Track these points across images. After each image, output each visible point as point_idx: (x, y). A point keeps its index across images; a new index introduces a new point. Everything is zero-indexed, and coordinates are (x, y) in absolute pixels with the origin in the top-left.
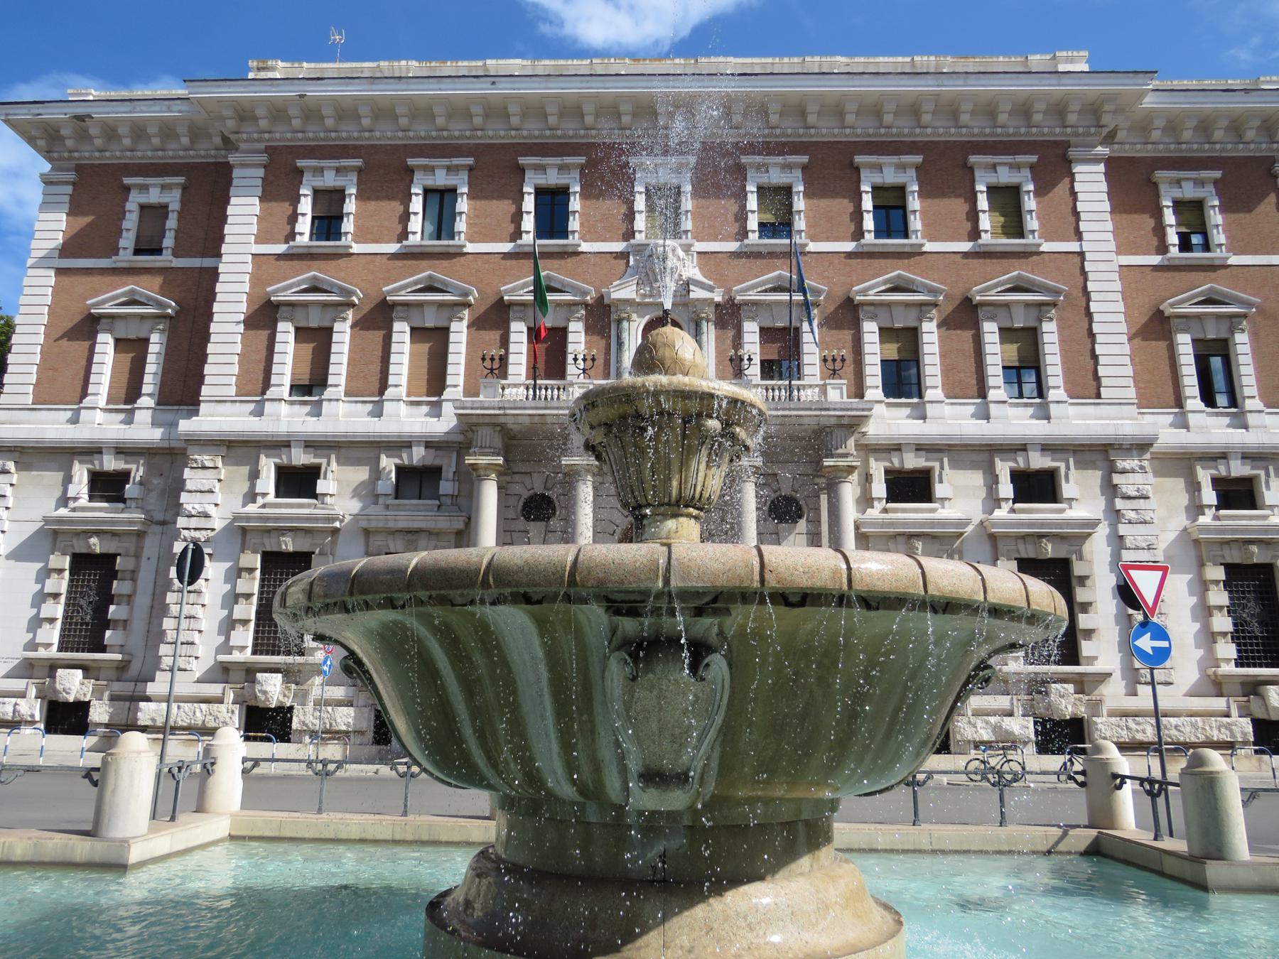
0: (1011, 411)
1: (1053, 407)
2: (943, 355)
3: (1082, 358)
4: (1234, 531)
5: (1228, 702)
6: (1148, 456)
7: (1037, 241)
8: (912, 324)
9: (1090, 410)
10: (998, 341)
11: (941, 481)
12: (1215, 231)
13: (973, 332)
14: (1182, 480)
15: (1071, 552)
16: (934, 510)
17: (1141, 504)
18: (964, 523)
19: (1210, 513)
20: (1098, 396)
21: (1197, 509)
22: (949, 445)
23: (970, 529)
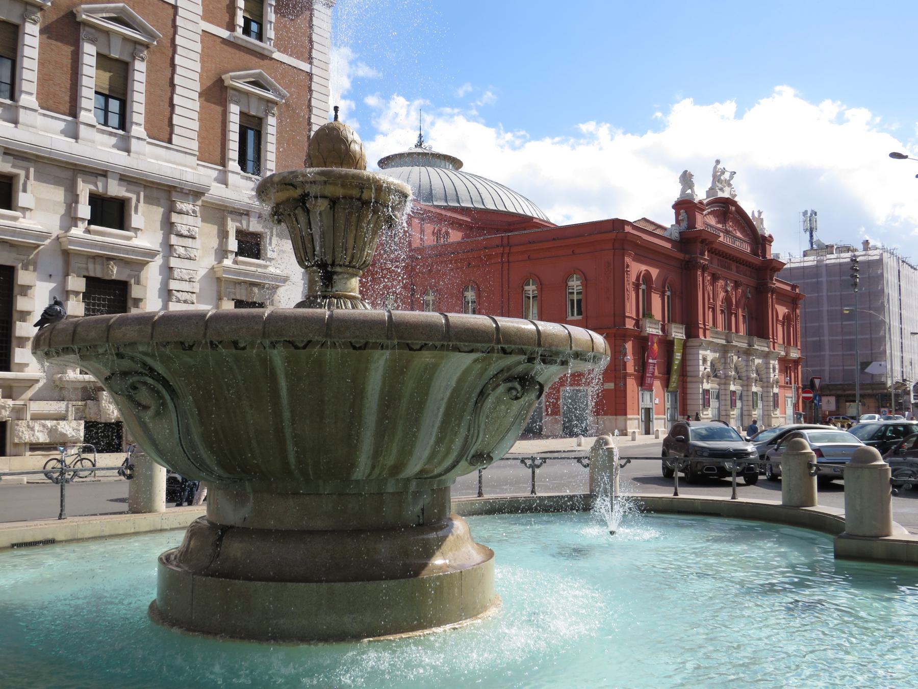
0: (100, 137)
1: (134, 142)
2: (41, 63)
3: (162, 103)
4: (246, 275)
5: (67, 407)
6: (199, 203)
7: (272, 48)
8: (15, 20)
9: (162, 152)
10: (94, 65)
11: (25, 191)
12: (269, 26)
13: (72, 48)
14: (216, 227)
15: (130, 276)
16: (15, 219)
17: (189, 242)
18: (43, 236)
19: (82, 226)
20: (170, 141)
21: (222, 253)
22: (37, 156)
23: (47, 242)
